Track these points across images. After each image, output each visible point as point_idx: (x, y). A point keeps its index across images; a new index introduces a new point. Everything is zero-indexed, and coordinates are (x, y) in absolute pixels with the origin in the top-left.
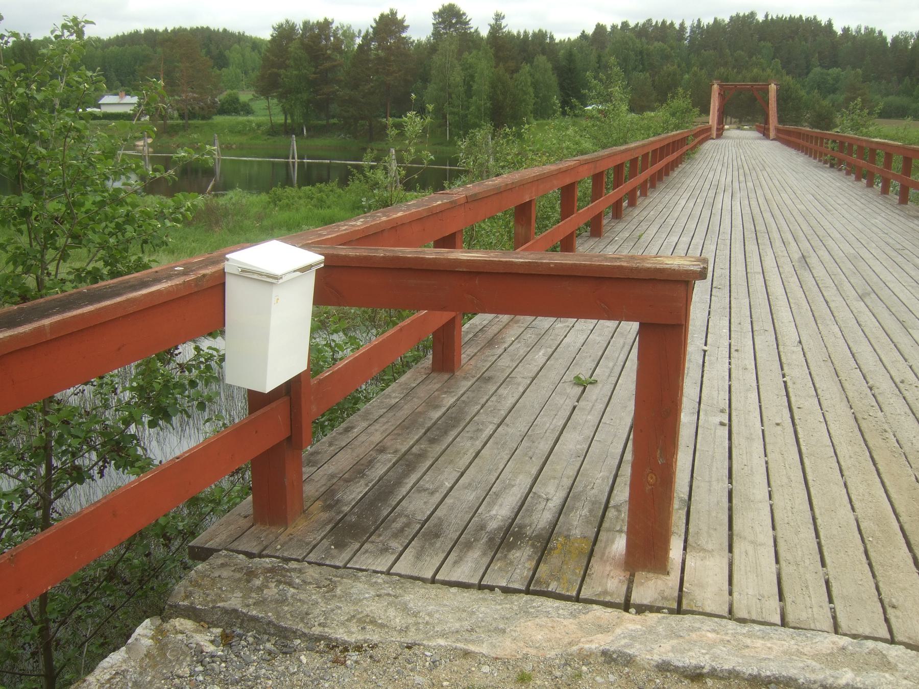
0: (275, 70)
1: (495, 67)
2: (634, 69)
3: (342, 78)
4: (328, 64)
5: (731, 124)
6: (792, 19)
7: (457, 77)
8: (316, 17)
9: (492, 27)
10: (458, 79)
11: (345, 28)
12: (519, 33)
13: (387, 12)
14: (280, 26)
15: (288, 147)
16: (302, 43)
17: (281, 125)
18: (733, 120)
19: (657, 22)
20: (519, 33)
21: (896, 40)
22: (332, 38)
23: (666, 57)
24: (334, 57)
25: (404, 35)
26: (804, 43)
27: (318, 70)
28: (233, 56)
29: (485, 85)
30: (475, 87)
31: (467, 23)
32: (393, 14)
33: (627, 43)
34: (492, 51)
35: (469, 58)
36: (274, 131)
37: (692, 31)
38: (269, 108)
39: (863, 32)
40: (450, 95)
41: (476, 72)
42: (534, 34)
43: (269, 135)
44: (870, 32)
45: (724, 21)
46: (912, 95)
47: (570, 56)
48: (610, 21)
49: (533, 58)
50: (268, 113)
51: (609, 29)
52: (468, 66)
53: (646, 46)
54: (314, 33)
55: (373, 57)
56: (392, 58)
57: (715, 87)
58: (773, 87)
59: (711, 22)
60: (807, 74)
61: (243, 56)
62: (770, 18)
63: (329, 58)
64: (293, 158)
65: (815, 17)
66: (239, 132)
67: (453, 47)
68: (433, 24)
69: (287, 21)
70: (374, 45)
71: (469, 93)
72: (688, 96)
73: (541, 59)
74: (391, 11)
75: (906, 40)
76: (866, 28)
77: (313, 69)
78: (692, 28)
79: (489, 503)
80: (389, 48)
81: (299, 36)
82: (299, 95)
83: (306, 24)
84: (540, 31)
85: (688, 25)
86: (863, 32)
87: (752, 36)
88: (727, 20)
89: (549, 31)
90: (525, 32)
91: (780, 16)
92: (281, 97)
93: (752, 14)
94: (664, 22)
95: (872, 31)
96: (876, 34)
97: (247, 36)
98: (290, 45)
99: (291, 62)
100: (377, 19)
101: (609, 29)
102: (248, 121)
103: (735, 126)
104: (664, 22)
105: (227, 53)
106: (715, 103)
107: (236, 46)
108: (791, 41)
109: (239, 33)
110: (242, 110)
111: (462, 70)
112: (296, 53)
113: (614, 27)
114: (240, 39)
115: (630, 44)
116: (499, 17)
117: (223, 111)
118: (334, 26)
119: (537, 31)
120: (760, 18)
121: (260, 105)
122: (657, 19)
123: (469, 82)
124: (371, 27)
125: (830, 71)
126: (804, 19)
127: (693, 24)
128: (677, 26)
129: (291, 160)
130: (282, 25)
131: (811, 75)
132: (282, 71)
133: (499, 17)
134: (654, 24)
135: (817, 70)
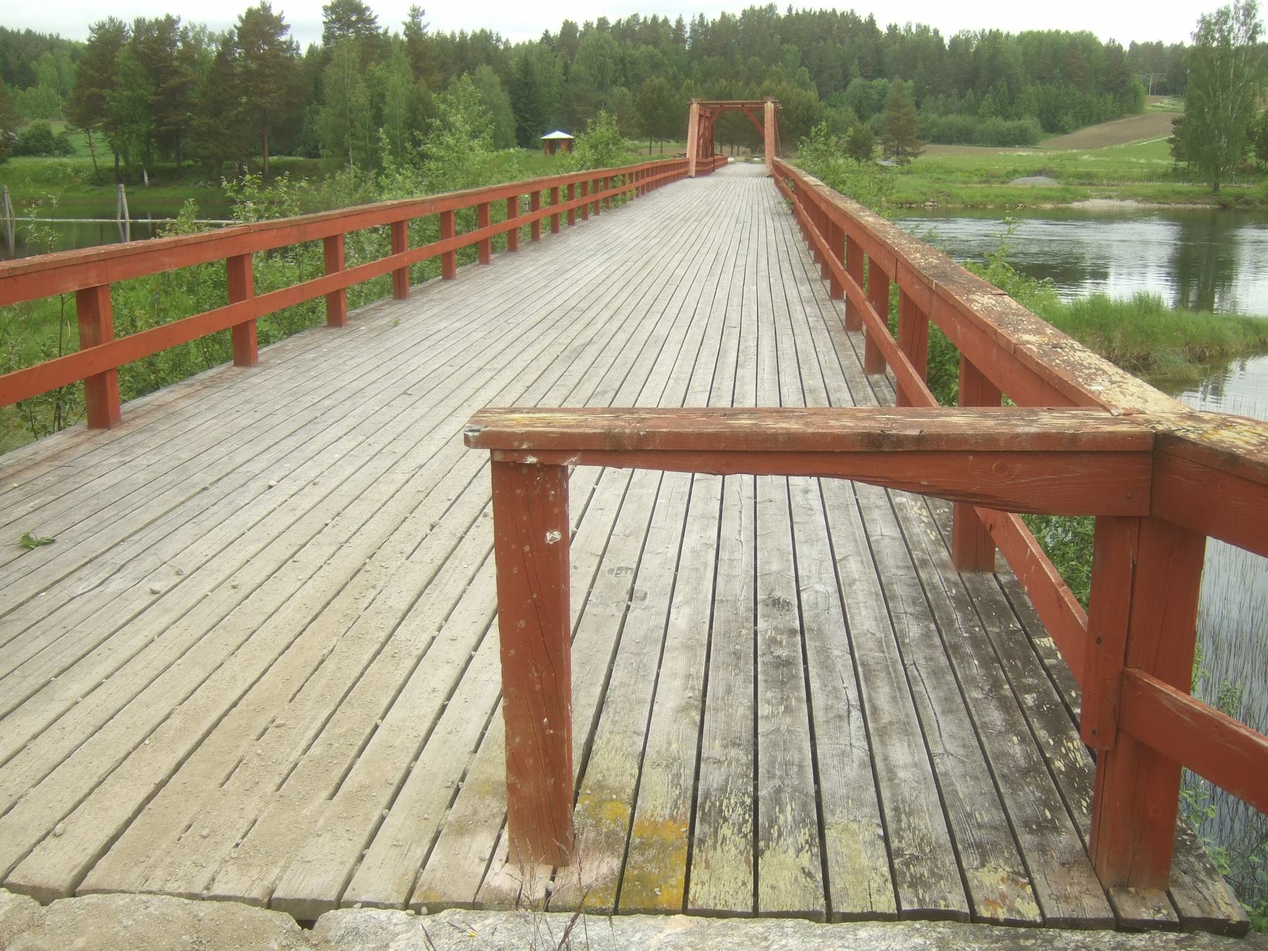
0: (95, 90)
1: (414, 83)
2: (614, 82)
3: (196, 101)
4: (174, 82)
5: (738, 155)
6: (823, 14)
7: (360, 96)
8: (154, 12)
9: (408, 27)
10: (362, 100)
11: (198, 29)
12: (453, 35)
13: (256, 5)
14: (101, 27)
15: (115, 202)
16: (135, 51)
17: (111, 170)
18: (742, 149)
19: (645, 18)
20: (453, 35)
21: (955, 41)
22: (179, 44)
23: (656, 66)
24: (183, 70)
25: (283, 38)
26: (839, 45)
27: (160, 90)
28: (44, 69)
29: (400, 107)
30: (386, 110)
31: (372, 21)
32: (266, 8)
33: (602, 47)
34: (409, 59)
35: (377, 70)
36: (101, 178)
37: (693, 30)
38: (91, 145)
39: (914, 30)
40: (352, 122)
41: (387, 90)
42: (474, 36)
43: (93, 184)
44: (923, 30)
45: (734, 16)
46: (977, 114)
47: (526, 67)
48: (584, 16)
49: (474, 69)
50: (90, 153)
51: (581, 28)
52: (375, 81)
53: (631, 51)
54: (152, 35)
55: (239, 69)
56: (267, 71)
57: (695, 107)
58: (769, 106)
59: (718, 18)
60: (845, 87)
61: (58, 69)
62: (794, 12)
63: (175, 72)
64: (123, 217)
65: (852, 11)
66: (48, 181)
67: (354, 54)
68: (324, 23)
69: (111, 20)
70: (238, 52)
71: (378, 119)
72: (614, 122)
73: (485, 70)
74: (263, 4)
75: (968, 40)
76: (918, 26)
77: (153, 89)
78: (693, 25)
79: (866, 680)
80: (261, 58)
81: (129, 40)
82: (134, 126)
83: (139, 23)
84: (482, 31)
85: (687, 22)
86: (914, 30)
87: (772, 36)
88: (739, 16)
89: (494, 32)
90: (462, 33)
91: (808, 10)
92: (106, 129)
93: (771, 8)
94: (655, 19)
95: (926, 29)
96: (931, 33)
97: (63, 41)
98: (117, 54)
99: (120, 79)
100: (244, 16)
101: (581, 28)
102: (61, 165)
103: (743, 158)
104: (655, 19)
105: (34, 65)
106: (693, 128)
107: (48, 55)
108: (822, 42)
109: (51, 35)
110: (56, 149)
111: (368, 87)
112: (125, 65)
113: (588, 26)
114: (52, 45)
115: (607, 47)
116: (416, 13)
117: (26, 149)
118: (181, 26)
119: (478, 31)
120: (782, 12)
121: (78, 139)
122: (645, 14)
123: (377, 103)
124: (235, 26)
125: (875, 82)
126: (838, 13)
127: (694, 21)
128: (673, 24)
129: (119, 221)
130: (104, 25)
131: (850, 88)
132: (107, 92)
133: (416, 13)
134: (642, 20)
135: (857, 81)
